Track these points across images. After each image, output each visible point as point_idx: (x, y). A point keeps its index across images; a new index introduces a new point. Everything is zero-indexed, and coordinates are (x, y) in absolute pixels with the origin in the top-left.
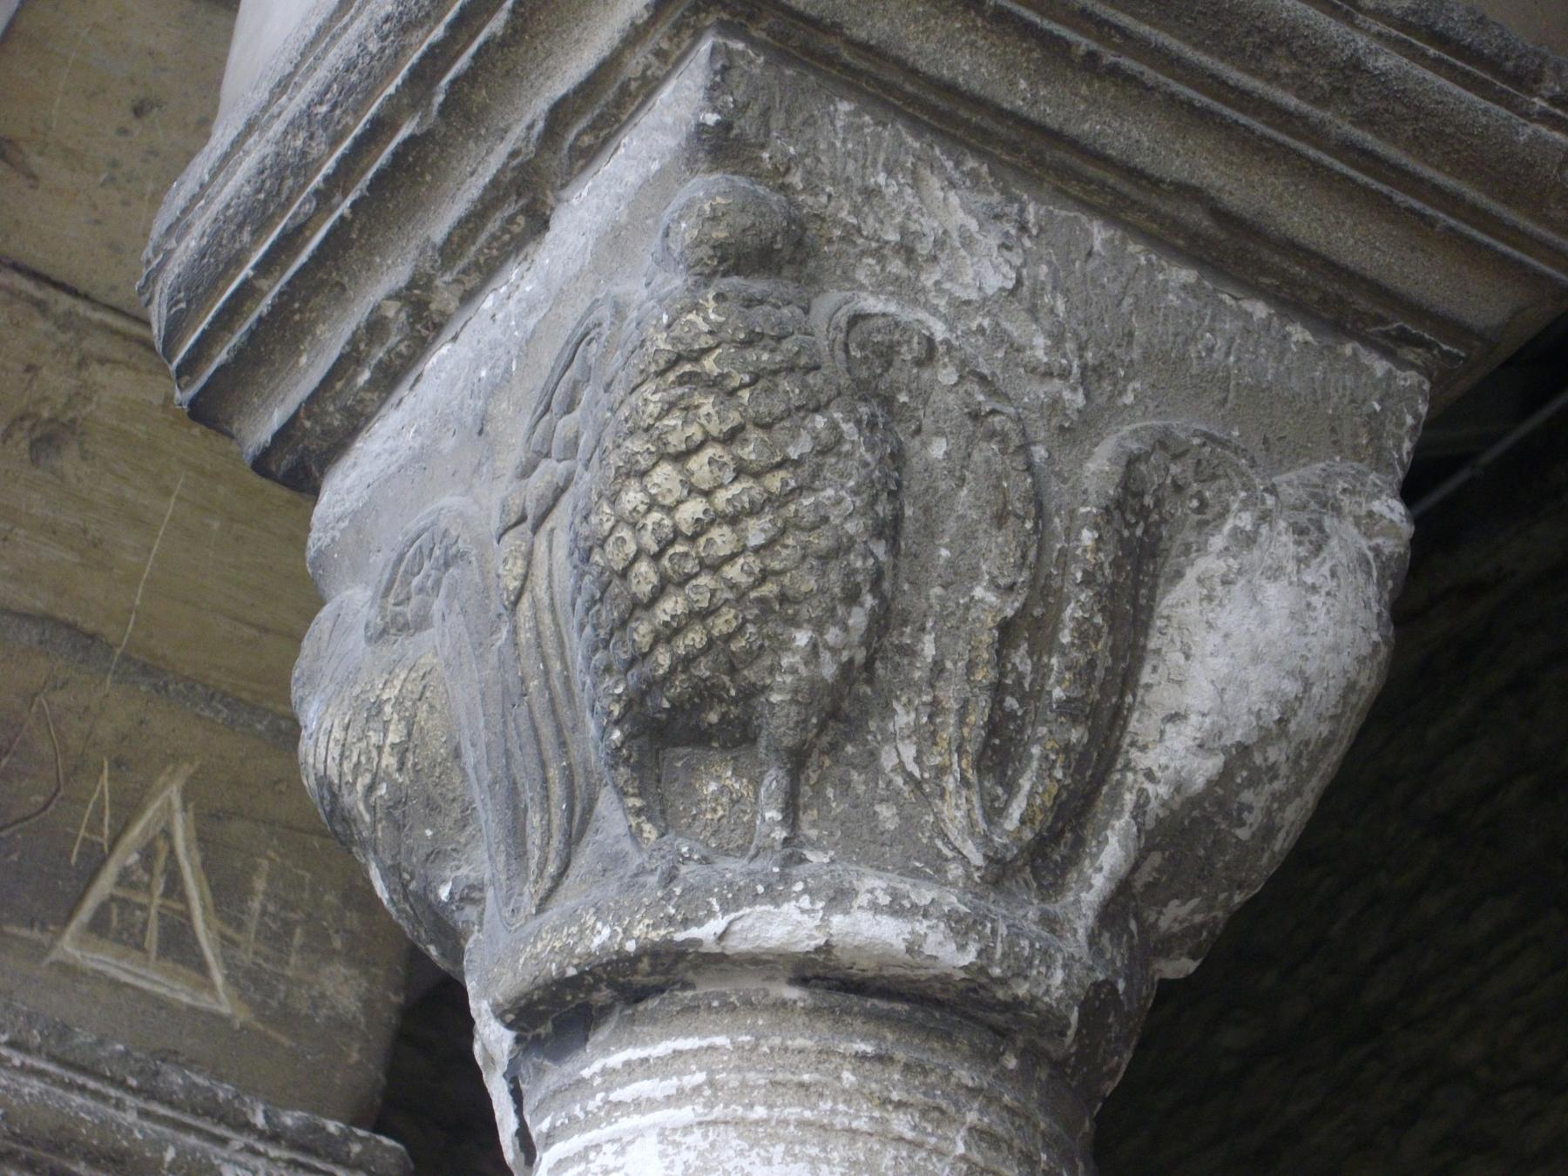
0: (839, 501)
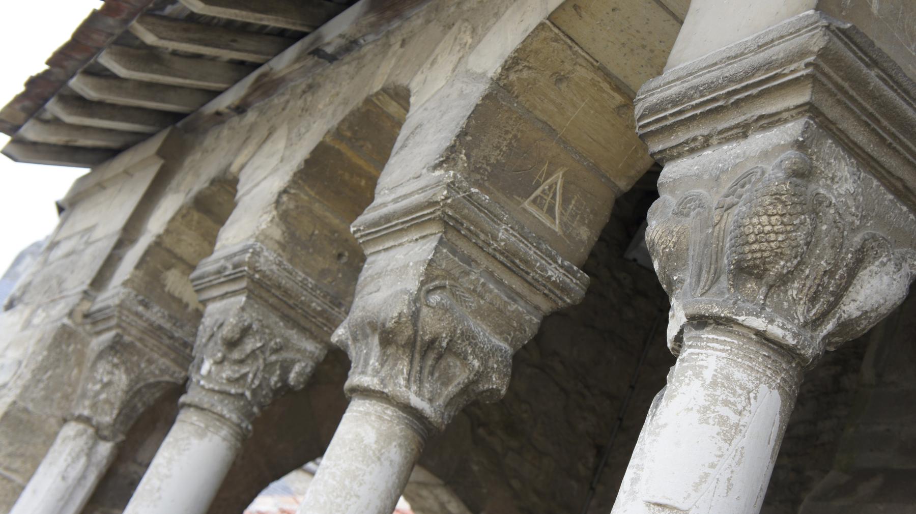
0: (800, 236)
